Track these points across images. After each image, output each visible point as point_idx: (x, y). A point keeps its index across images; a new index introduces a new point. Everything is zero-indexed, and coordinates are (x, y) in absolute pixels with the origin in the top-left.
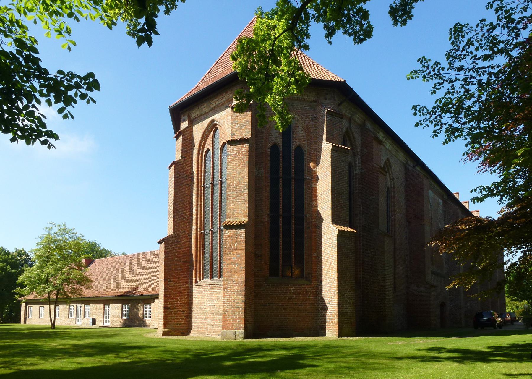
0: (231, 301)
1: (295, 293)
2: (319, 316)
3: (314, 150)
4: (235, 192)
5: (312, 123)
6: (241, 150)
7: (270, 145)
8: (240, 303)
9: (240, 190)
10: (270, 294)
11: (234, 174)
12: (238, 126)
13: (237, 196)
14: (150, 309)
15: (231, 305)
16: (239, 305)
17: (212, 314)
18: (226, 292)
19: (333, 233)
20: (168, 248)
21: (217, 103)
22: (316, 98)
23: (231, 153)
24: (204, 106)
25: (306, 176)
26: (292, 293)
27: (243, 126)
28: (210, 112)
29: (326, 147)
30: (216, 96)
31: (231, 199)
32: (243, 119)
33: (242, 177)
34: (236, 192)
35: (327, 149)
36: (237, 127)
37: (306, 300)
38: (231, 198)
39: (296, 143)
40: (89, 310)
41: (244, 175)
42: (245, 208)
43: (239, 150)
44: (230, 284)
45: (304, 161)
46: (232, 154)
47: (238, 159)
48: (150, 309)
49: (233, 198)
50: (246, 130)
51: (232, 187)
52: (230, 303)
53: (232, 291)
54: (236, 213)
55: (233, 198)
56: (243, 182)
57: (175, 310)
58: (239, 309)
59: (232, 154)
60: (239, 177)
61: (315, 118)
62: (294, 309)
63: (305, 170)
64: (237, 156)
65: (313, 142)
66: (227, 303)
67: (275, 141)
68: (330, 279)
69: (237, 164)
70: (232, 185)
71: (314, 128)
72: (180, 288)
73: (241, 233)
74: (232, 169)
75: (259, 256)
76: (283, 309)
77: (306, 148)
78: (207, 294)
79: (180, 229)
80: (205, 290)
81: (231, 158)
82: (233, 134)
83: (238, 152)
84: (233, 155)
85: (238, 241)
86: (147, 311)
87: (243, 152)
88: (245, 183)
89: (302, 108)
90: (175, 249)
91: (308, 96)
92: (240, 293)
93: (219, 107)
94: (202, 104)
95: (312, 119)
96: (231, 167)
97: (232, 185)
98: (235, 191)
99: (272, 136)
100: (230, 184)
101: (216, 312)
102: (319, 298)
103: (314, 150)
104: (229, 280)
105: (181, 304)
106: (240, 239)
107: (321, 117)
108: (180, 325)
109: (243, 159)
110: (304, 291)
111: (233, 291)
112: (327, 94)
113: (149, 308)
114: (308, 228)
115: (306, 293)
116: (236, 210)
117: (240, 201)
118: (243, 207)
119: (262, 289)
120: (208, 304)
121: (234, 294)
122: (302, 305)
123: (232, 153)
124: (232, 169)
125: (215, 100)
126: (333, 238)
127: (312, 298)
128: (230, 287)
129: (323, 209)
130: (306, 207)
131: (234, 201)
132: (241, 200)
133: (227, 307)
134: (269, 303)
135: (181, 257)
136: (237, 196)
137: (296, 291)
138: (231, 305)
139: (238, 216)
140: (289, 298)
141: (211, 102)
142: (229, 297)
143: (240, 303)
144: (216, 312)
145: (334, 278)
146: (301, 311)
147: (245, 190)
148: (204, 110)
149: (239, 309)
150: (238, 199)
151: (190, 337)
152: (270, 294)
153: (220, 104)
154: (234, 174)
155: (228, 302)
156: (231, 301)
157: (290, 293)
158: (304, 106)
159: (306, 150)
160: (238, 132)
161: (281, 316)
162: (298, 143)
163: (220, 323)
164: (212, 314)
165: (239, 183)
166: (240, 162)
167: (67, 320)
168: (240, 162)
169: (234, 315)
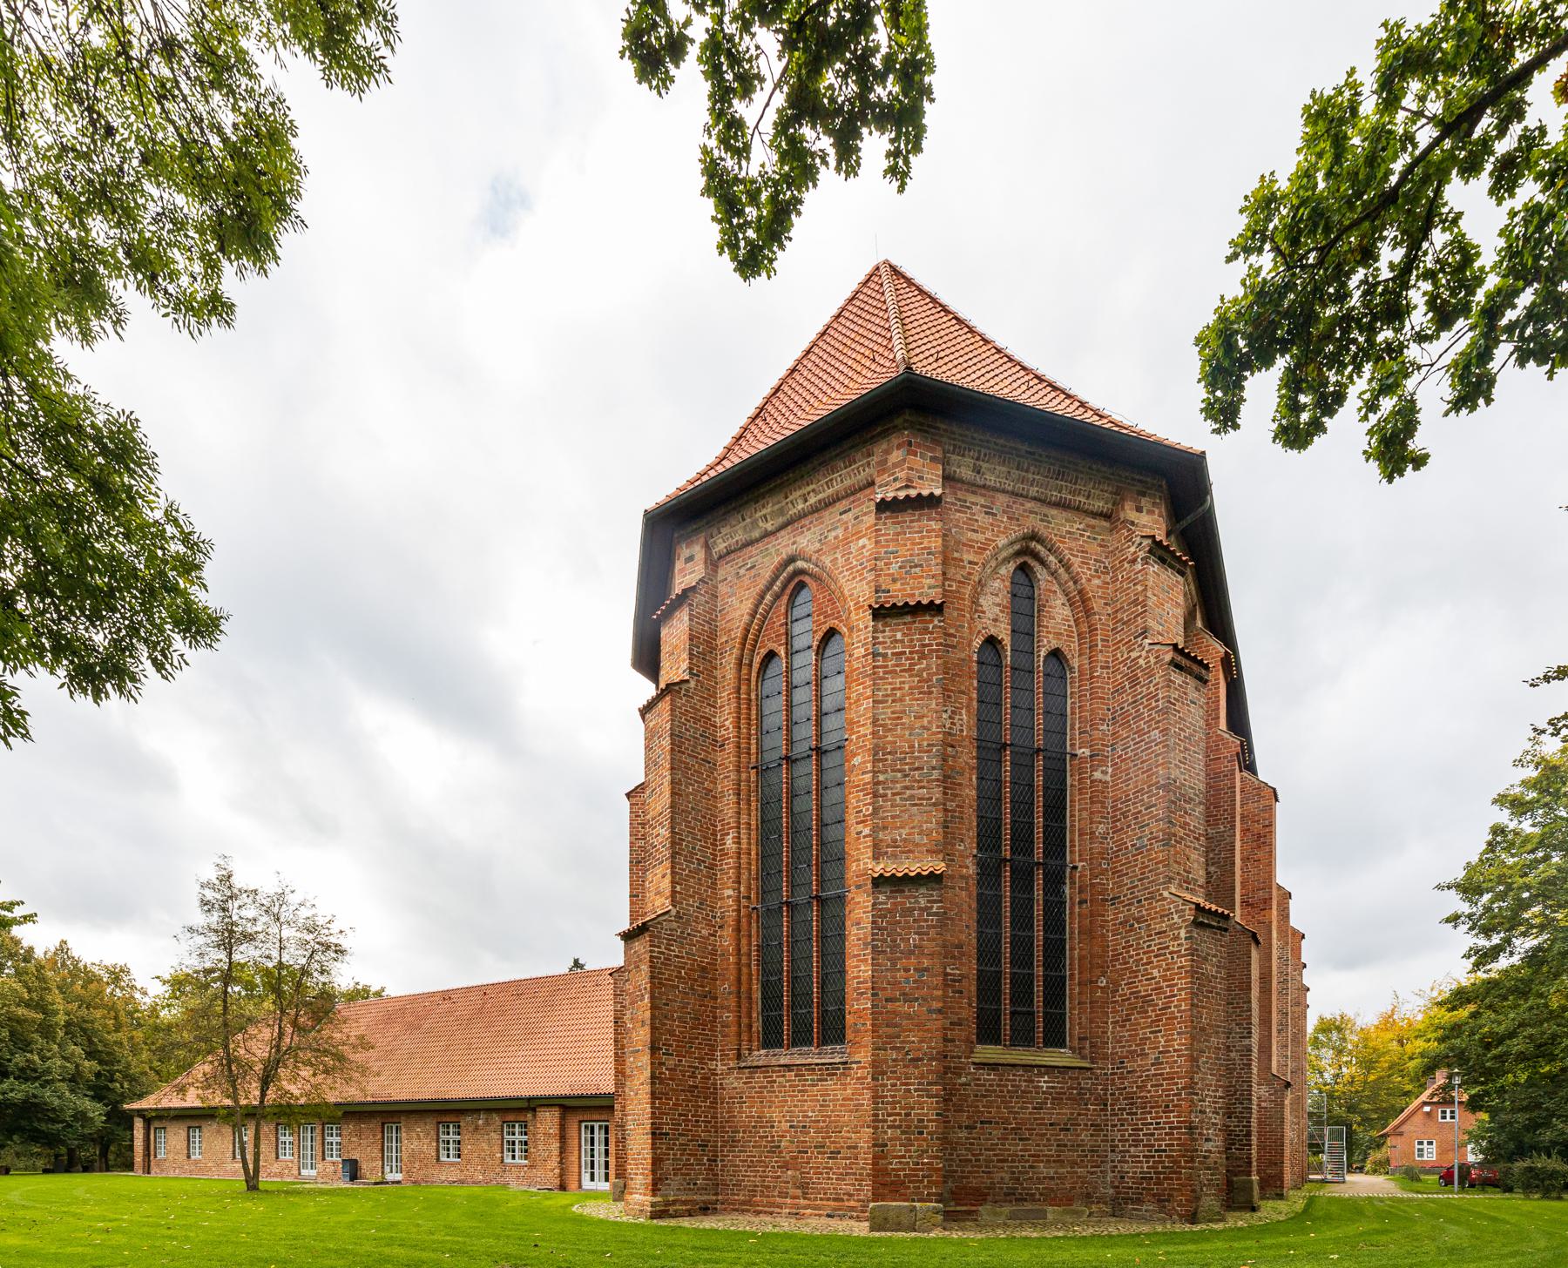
0: (900, 1114)
1: (1051, 1094)
2: (1113, 1161)
3: (1102, 668)
4: (899, 775)
5: (1096, 582)
6: (919, 640)
7: (977, 642)
8: (929, 1121)
9: (917, 769)
10: (985, 1096)
11: (898, 718)
12: (900, 567)
13: (907, 788)
14: (524, 1138)
15: (900, 1127)
16: (926, 1127)
17: (800, 1152)
18: (882, 1085)
19: (1175, 916)
20: (659, 953)
21: (812, 500)
22: (1110, 506)
23: (885, 648)
24: (764, 512)
25: (1072, 745)
26: (1044, 1093)
27: (916, 566)
28: (783, 533)
29: (1147, 657)
30: (802, 479)
31: (886, 795)
32: (913, 544)
33: (924, 728)
34: (906, 776)
35: (1152, 660)
36: (894, 568)
37: (1079, 1114)
38: (889, 792)
39: (1049, 642)
40: (339, 1139)
41: (929, 722)
42: (933, 826)
43: (912, 640)
44: (894, 1060)
45: (1069, 702)
46: (889, 652)
47: (910, 670)
48: (524, 1138)
49: (894, 794)
50: (924, 581)
51: (889, 757)
52: (895, 1120)
53: (902, 1084)
54: (905, 840)
55: (894, 794)
56: (925, 743)
57: (682, 1140)
58: (925, 1140)
59: (889, 652)
60: (912, 728)
61: (1105, 567)
62: (1048, 1140)
63: (1072, 728)
64: (907, 659)
65: (1100, 643)
66: (886, 1121)
67: (993, 631)
68: (1160, 1053)
69: (907, 686)
70: (889, 753)
71: (1101, 597)
72: (693, 1076)
73: (929, 901)
74: (890, 699)
75: (954, 981)
76: (1020, 1139)
77: (1075, 663)
78: (780, 1092)
79: (691, 896)
80: (775, 1082)
81: (887, 666)
82: (884, 591)
83: (910, 647)
84: (893, 654)
85: (920, 927)
86: (514, 1143)
87: (924, 646)
88: (933, 745)
89: (1070, 533)
90: (677, 956)
91: (1088, 498)
92: (927, 1090)
93: (816, 515)
94: (757, 502)
95: (1096, 571)
96: (887, 696)
97: (889, 753)
98: (900, 771)
99: (984, 612)
100: (884, 748)
101: (815, 1147)
102: (1113, 1110)
103: (1102, 668)
104: (891, 1049)
105: (697, 1121)
106: (927, 921)
107: (1126, 565)
108: (695, 1184)
109: (924, 670)
110: (1073, 1089)
111: (906, 1084)
112: (1143, 494)
113: (521, 1133)
114: (1081, 903)
115: (1079, 1094)
116: (904, 832)
117: (916, 805)
118: (926, 822)
119: (964, 1080)
120: (787, 1121)
121: (909, 1090)
122: (1068, 1130)
123: (888, 648)
124: (890, 699)
125: (805, 490)
126: (1176, 932)
127: (1095, 1110)
128: (895, 1072)
129: (1133, 846)
130: (1072, 841)
131: (898, 801)
132: (919, 799)
133: (886, 1133)
134: (982, 1122)
135: (696, 980)
136: (907, 788)
137: (1053, 1088)
138: (900, 1127)
139: (910, 851)
140: (1035, 1108)
141: (791, 498)
142: (894, 1103)
143: (929, 1121)
144: (815, 1147)
145: (1175, 1051)
146: (1065, 1146)
147: (934, 768)
148: (761, 524)
149: (925, 1140)
150: (912, 797)
151: (1260, 1219)
152: (985, 1096)
153: (820, 501)
154: (898, 718)
155: (889, 1115)
156: (900, 1114)
157: (1037, 1093)
158: (1077, 526)
159: (1076, 666)
160: (898, 585)
161: (1014, 1161)
162: (1054, 644)
163: (829, 1178)
164: (800, 1152)
165: (913, 746)
166: (916, 679)
167: (271, 1164)
168: (916, 679)
169: (910, 1157)
